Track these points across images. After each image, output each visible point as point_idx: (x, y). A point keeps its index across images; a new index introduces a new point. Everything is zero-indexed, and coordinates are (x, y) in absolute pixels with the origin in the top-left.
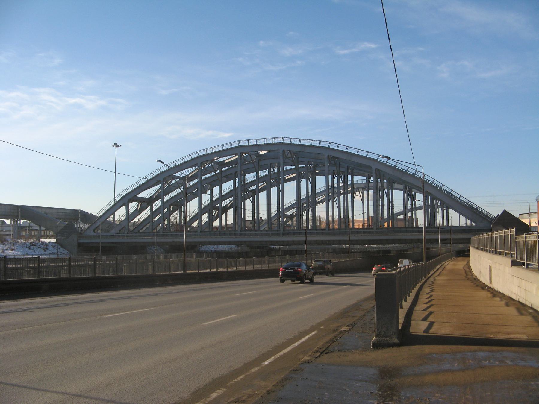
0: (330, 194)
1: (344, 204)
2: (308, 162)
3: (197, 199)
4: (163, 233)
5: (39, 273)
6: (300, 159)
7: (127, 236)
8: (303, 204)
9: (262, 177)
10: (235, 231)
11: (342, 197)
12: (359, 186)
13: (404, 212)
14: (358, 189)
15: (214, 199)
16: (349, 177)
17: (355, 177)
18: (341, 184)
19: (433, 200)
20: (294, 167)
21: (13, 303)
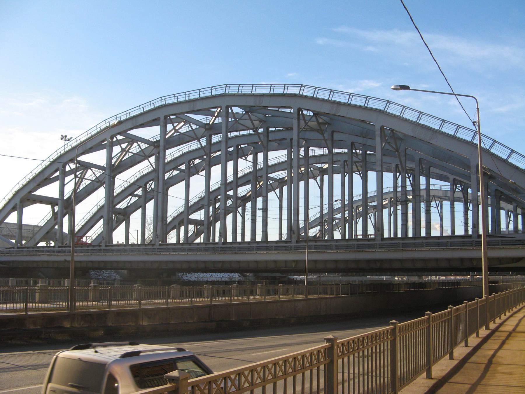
0: (399, 199)
1: (493, 222)
2: (353, 143)
3: (184, 182)
4: (106, 246)
5: (231, 302)
6: (337, 136)
7: (17, 252)
8: (357, 207)
9: (215, 143)
10: (100, 246)
11: (410, 205)
12: (436, 194)
13: (321, 221)
14: (435, 198)
15: (213, 187)
16: (423, 180)
17: (432, 181)
18: (409, 188)
19: (153, 176)
20: (346, 151)
21: (224, 343)
